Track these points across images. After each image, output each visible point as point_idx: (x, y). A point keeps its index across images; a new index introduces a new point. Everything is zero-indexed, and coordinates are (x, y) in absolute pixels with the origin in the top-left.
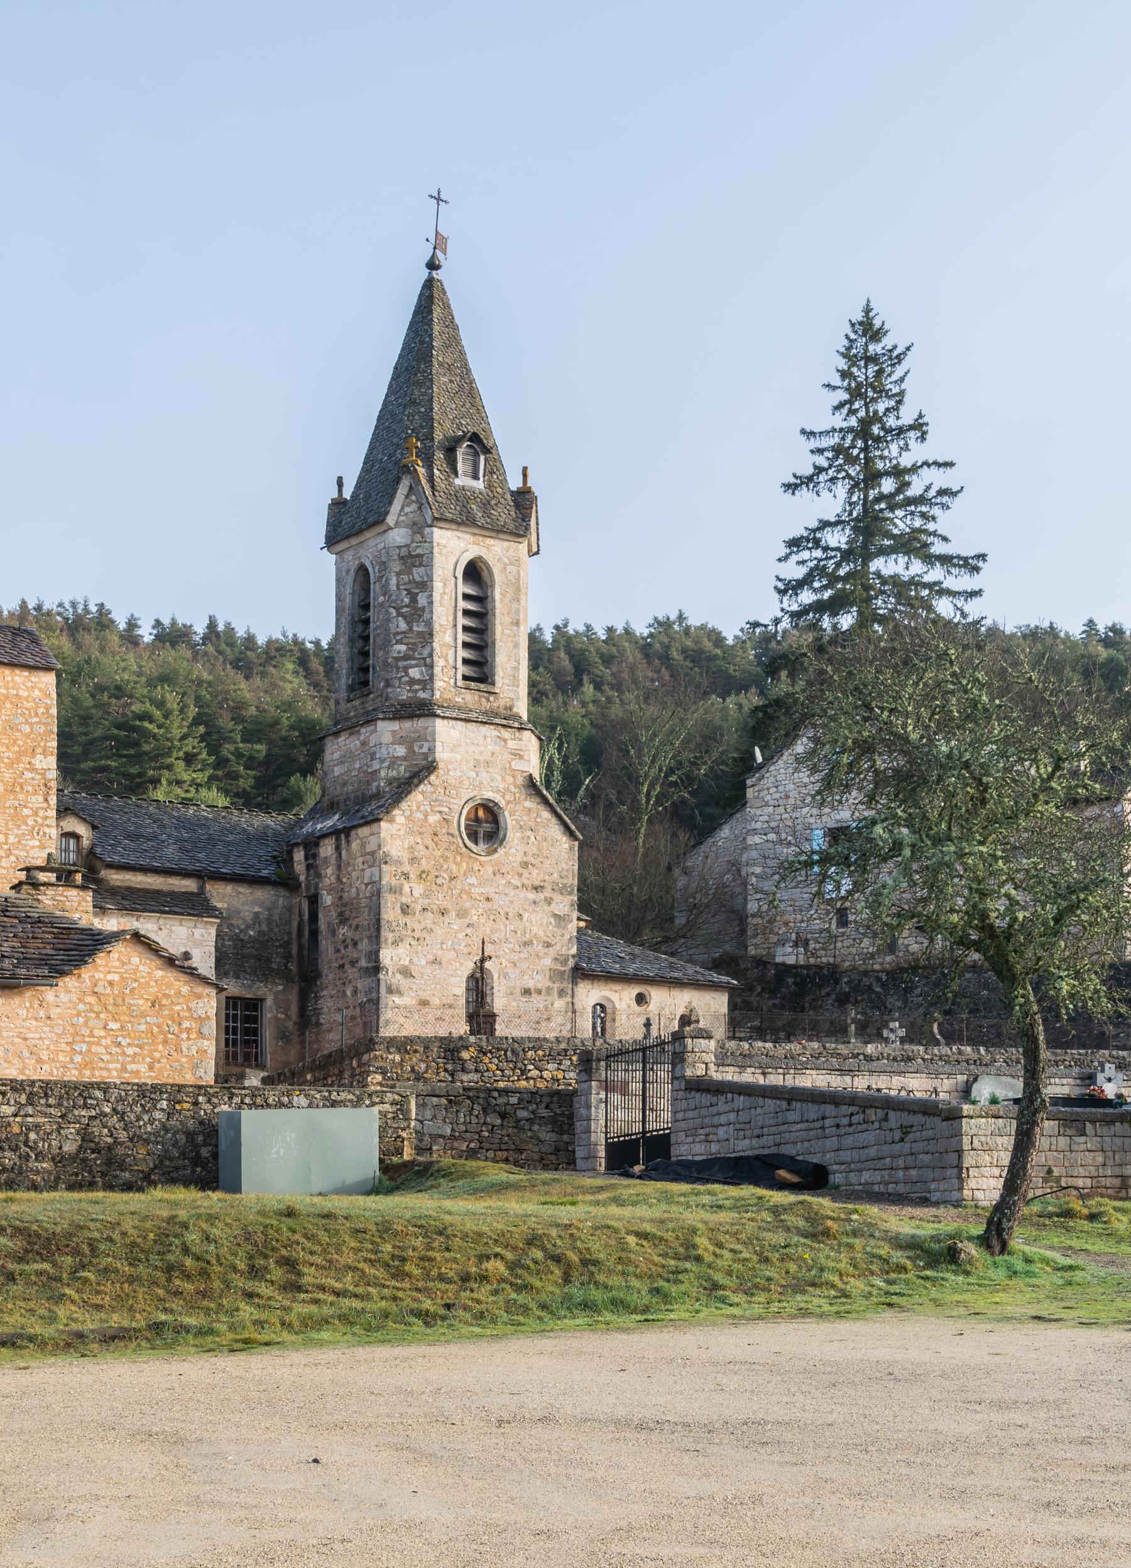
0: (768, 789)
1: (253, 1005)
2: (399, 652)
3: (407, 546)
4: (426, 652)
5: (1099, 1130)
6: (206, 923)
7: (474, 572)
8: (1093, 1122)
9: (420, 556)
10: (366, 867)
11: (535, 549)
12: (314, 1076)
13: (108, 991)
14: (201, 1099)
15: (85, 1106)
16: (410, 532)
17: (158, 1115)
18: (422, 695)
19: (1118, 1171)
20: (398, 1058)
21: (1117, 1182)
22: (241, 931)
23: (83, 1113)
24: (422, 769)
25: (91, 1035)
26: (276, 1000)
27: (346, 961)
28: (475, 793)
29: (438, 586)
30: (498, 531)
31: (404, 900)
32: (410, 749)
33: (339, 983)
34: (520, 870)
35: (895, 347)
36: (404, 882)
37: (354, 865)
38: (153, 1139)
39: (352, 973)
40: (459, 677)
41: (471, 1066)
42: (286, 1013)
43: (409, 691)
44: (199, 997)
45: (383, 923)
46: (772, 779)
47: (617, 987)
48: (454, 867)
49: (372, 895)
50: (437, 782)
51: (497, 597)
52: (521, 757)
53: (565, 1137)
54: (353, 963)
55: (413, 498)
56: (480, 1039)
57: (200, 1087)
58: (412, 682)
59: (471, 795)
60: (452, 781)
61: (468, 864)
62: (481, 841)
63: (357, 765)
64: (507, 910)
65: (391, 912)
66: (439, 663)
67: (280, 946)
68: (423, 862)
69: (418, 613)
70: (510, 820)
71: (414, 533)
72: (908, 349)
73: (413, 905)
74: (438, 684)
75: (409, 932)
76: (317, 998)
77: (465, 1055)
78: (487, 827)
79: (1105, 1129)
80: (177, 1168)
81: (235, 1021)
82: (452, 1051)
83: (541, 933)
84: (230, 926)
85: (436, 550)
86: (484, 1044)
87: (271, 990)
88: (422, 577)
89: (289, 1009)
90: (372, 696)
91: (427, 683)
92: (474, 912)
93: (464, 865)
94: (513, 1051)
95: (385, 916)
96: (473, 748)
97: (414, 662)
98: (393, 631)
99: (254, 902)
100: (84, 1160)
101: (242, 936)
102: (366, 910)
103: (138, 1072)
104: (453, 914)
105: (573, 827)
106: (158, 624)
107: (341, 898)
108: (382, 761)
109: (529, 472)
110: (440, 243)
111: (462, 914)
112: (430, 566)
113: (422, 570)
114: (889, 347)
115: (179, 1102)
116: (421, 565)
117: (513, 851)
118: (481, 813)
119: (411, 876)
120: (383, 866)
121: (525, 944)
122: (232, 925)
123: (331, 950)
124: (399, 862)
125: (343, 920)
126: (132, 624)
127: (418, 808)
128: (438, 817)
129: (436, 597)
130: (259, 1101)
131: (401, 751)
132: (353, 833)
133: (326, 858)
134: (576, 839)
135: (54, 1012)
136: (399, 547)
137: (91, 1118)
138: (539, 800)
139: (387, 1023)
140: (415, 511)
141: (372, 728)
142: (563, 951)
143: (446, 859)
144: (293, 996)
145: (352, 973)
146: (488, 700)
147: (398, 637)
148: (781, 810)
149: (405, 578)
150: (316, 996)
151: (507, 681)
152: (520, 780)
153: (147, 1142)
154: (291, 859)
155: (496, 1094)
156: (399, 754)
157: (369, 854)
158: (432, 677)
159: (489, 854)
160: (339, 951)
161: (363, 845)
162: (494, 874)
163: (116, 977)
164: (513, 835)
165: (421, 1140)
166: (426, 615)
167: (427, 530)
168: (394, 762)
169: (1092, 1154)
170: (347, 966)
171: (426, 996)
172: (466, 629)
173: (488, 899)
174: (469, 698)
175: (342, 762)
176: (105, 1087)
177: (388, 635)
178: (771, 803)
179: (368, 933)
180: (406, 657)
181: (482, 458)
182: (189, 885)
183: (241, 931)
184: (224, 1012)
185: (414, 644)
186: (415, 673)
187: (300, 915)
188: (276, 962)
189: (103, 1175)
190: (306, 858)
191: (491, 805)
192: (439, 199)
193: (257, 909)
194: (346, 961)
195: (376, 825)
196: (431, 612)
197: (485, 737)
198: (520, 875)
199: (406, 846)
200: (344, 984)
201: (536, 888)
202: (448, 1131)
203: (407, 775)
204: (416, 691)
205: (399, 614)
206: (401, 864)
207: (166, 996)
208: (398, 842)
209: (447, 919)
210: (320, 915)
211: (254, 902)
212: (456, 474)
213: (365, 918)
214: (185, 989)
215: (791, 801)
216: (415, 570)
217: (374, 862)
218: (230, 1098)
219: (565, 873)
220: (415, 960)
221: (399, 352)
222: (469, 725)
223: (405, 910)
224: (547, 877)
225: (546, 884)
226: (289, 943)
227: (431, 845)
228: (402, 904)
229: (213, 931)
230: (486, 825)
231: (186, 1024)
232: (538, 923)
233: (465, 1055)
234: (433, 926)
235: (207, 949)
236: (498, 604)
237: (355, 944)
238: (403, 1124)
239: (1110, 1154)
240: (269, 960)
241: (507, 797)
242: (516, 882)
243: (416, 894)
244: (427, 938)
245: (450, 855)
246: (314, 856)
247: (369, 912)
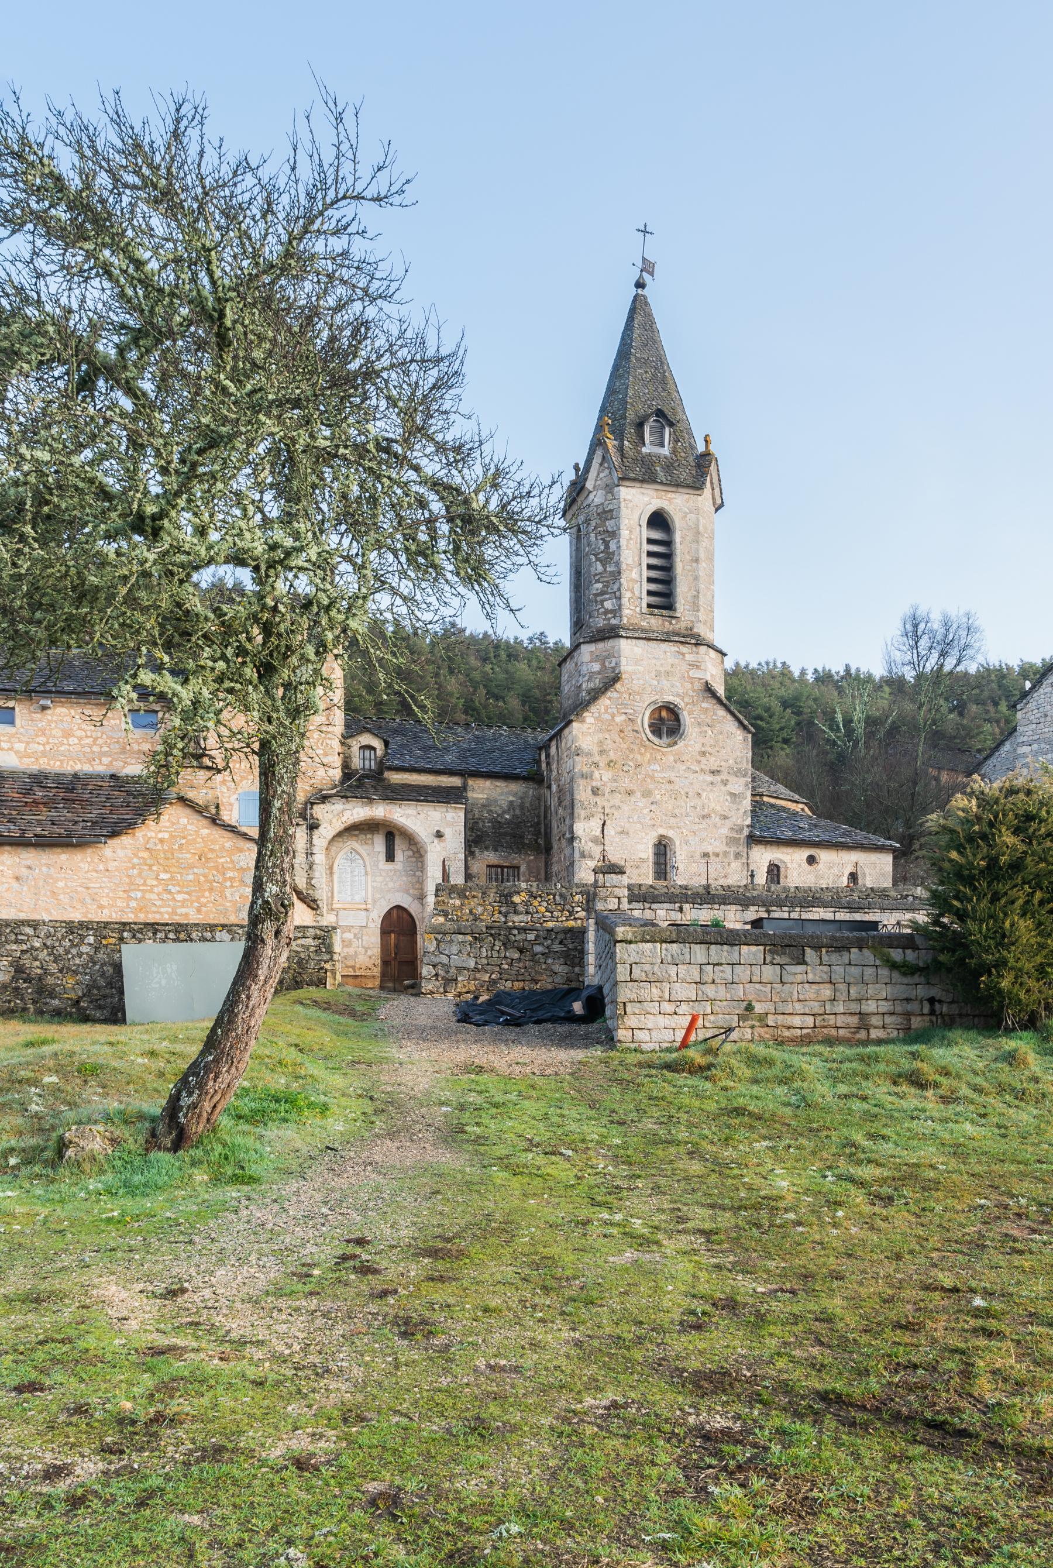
5: (825, 957)
7: (659, 520)
8: (817, 948)
9: (611, 511)
11: (719, 502)
13: (159, 847)
14: (125, 934)
15: (16, 942)
17: (84, 949)
18: (613, 622)
19: (854, 1007)
20: (458, 902)
21: (854, 1021)
23: (14, 947)
24: (613, 679)
25: (144, 884)
26: (528, 866)
29: (624, 533)
30: (678, 486)
31: (594, 784)
32: (603, 665)
38: (81, 970)
40: (644, 605)
41: (521, 908)
44: (241, 850)
47: (789, 850)
48: (639, 757)
50: (623, 690)
52: (698, 667)
53: (577, 969)
57: (124, 924)
58: (607, 612)
60: (636, 688)
65: (583, 794)
66: (626, 595)
68: (611, 753)
70: (686, 718)
74: (626, 612)
77: (517, 899)
79: (834, 958)
80: (105, 997)
82: (506, 896)
83: (718, 808)
85: (622, 505)
86: (534, 890)
89: (539, 874)
91: (617, 612)
93: (648, 755)
94: (561, 895)
95: (577, 797)
99: (509, 793)
100: (17, 989)
103: (186, 914)
105: (746, 723)
106: (816, 670)
109: (711, 438)
110: (648, 267)
111: (646, 794)
112: (618, 518)
115: (105, 938)
118: (664, 714)
121: (704, 817)
124: (589, 754)
126: (803, 672)
128: (624, 717)
130: (182, 936)
134: (749, 732)
135: (112, 866)
137: (23, 952)
142: (739, 822)
143: (632, 751)
148: (1041, 726)
152: (698, 686)
153: (76, 973)
155: (515, 932)
158: (620, 606)
159: (670, 746)
163: (166, 836)
165: (447, 972)
166: (616, 558)
169: (814, 986)
172: (650, 567)
174: (655, 623)
176: (34, 925)
180: (602, 593)
181: (667, 430)
182: (456, 781)
186: (608, 605)
188: (528, 838)
189: (35, 1002)
192: (645, 232)
193: (511, 798)
198: (699, 762)
202: (472, 964)
205: (597, 559)
207: (211, 850)
208: (589, 738)
209: (633, 799)
211: (509, 793)
212: (644, 444)
214: (228, 845)
218: (155, 934)
221: (663, 336)
222: (651, 643)
223: (595, 792)
226: (538, 823)
229: (462, 814)
230: (667, 723)
231: (230, 874)
232: (716, 800)
233: (517, 899)
238: (326, 957)
239: (842, 987)
240: (522, 837)
243: (605, 778)
245: (635, 747)
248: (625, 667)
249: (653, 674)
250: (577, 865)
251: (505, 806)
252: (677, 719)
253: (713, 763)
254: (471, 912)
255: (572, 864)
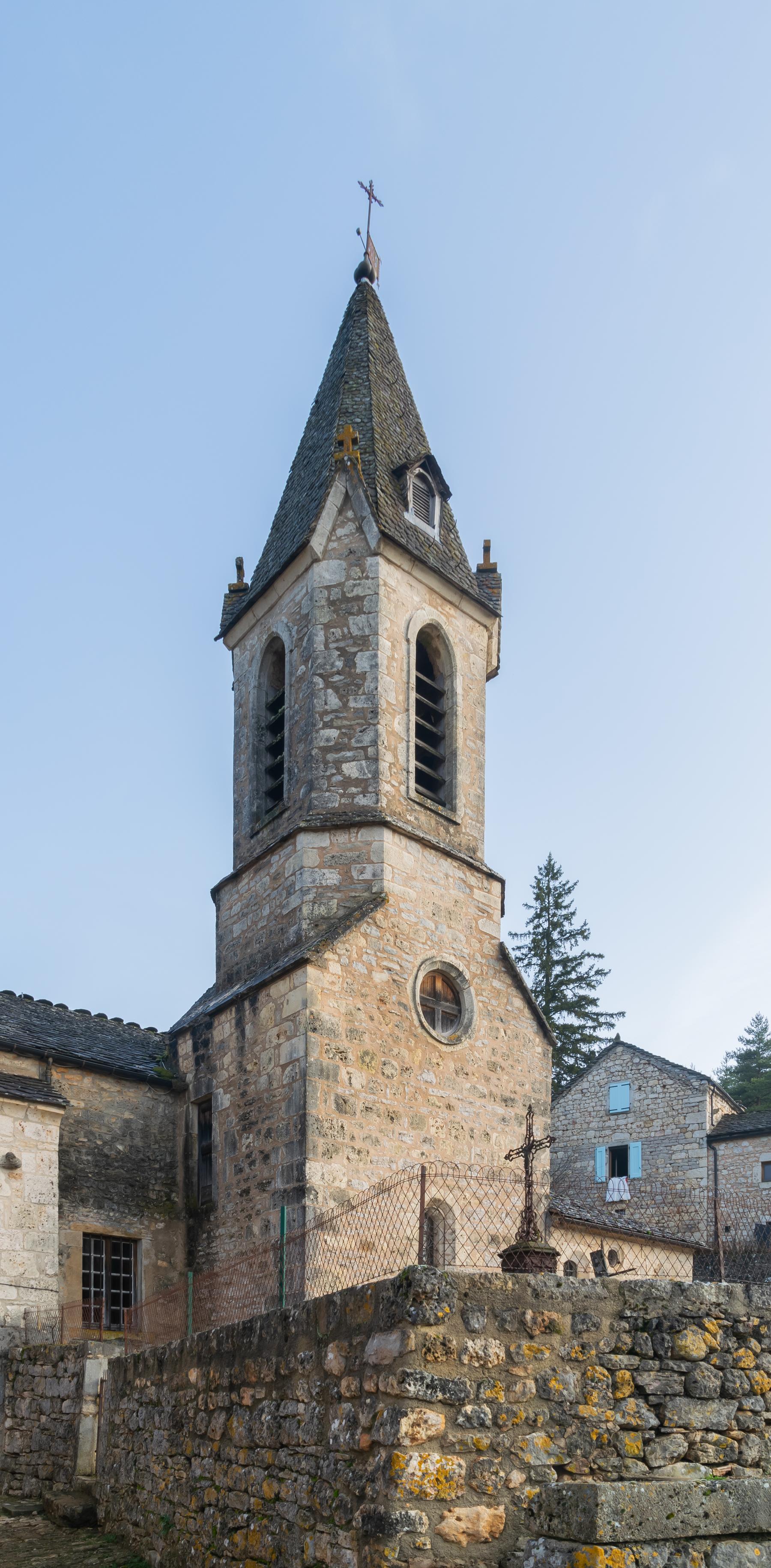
0: (558, 1117)
1: (125, 1247)
2: (328, 740)
3: (340, 585)
4: (367, 738)
6: (44, 1113)
7: (430, 652)
10: (282, 1039)
12: (205, 1376)
16: (344, 564)
20: (496, 1350)
22: (105, 1143)
24: (366, 903)
26: (155, 1241)
27: (252, 1184)
28: (433, 952)
29: (385, 643)
31: (340, 1090)
33: (241, 1216)
34: (489, 1073)
35: (568, 882)
36: (340, 1063)
37: (263, 1042)
39: (261, 1200)
42: (168, 1259)
43: (342, 796)
45: (310, 1121)
46: (562, 1109)
48: (405, 1053)
49: (294, 1080)
50: (384, 924)
51: (459, 690)
54: (263, 1186)
55: (350, 514)
56: (730, 1293)
58: (348, 782)
59: (429, 954)
61: (424, 1052)
62: (439, 1024)
63: (266, 912)
64: (471, 1125)
65: (322, 1106)
67: (161, 1169)
68: (366, 1037)
69: (354, 682)
71: (351, 565)
72: (575, 884)
73: (352, 1100)
75: (347, 1140)
76: (210, 1239)
77: (694, 1343)
78: (446, 1006)
81: (98, 1267)
84: (89, 1134)
85: (382, 591)
87: (148, 1227)
88: (362, 629)
90: (286, 815)
91: (369, 783)
92: (431, 1122)
93: (419, 1052)
96: (432, 887)
97: (349, 754)
98: (319, 709)
101: (106, 1150)
102: (283, 1105)
104: (405, 1121)
107: (244, 1094)
108: (304, 892)
111: (417, 1122)
113: (361, 619)
114: (564, 882)
116: (360, 612)
117: (479, 1044)
118: (439, 985)
119: (350, 1056)
120: (309, 1033)
122: (92, 1133)
123: (230, 1170)
125: (247, 1124)
127: (360, 956)
129: (383, 658)
131: (332, 877)
132: (262, 997)
133: (222, 1042)
136: (328, 588)
138: (509, 981)
139: (317, 1273)
140: (352, 534)
141: (290, 848)
143: (397, 1040)
144: (179, 1238)
145: (261, 1200)
146: (448, 832)
147: (327, 719)
148: (569, 1133)
149: (338, 632)
150: (209, 1237)
151: (469, 811)
152: (490, 949)
154: (175, 1054)
156: (329, 882)
157: (287, 1019)
158: (376, 774)
160: (241, 1170)
161: (279, 1009)
162: (457, 1073)
164: (480, 1023)
166: (368, 685)
167: (370, 560)
168: (322, 893)
170: (254, 1192)
171: (369, 1235)
173: (449, 1107)
174: (421, 820)
175: (245, 915)
177: (312, 716)
178: (561, 1128)
179: (286, 1140)
180: (338, 747)
182: (28, 1068)
183: (105, 1143)
184: (81, 1254)
185: (350, 727)
186: (351, 769)
187: (187, 1128)
188: (155, 1191)
190: (195, 1049)
191: (453, 975)
193: (127, 1115)
194: (252, 1184)
195: (299, 972)
196: (376, 679)
197: (447, 876)
198: (488, 1080)
199: (343, 1010)
200: (249, 1217)
201: (505, 1101)
203: (341, 913)
204: (353, 796)
205: (328, 685)
206: (336, 1036)
210: (215, 1124)
213: (281, 1117)
215: (578, 1126)
216: (351, 619)
217: (296, 1029)
219: (537, 1086)
220: (355, 1182)
223: (342, 1105)
224: (518, 1088)
225: (517, 1097)
226: (172, 1166)
227: (377, 1015)
228: (337, 1096)
229: (55, 1129)
230: (443, 1000)
233: (694, 1343)
234: (379, 1135)
235: (45, 1155)
236: (460, 699)
237: (266, 1157)
240: (144, 1187)
241: (473, 968)
242: (483, 1088)
243: (357, 1083)
244: (372, 1151)
246: (206, 1043)
247: (288, 1107)
248: (391, 884)
249: (430, 909)
250: (310, 1238)
251: (117, 1127)
252: (457, 998)
253: (505, 1084)
254: (544, 1393)
255: (303, 1236)
